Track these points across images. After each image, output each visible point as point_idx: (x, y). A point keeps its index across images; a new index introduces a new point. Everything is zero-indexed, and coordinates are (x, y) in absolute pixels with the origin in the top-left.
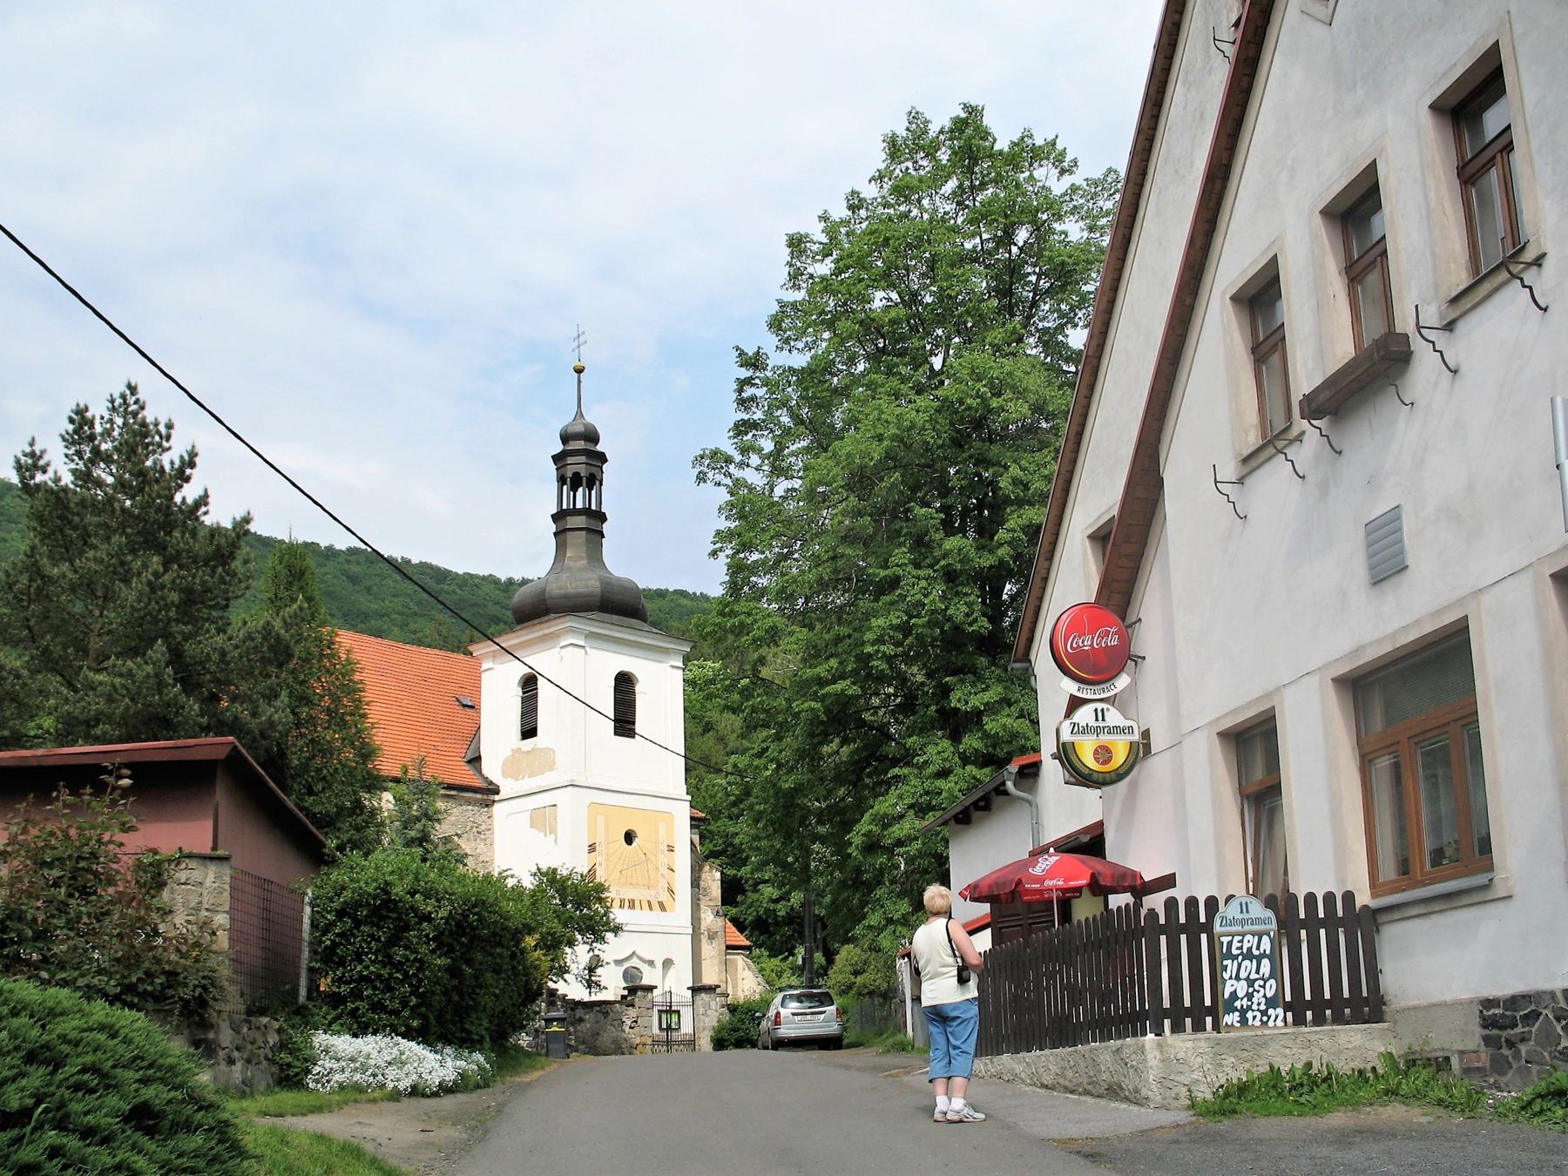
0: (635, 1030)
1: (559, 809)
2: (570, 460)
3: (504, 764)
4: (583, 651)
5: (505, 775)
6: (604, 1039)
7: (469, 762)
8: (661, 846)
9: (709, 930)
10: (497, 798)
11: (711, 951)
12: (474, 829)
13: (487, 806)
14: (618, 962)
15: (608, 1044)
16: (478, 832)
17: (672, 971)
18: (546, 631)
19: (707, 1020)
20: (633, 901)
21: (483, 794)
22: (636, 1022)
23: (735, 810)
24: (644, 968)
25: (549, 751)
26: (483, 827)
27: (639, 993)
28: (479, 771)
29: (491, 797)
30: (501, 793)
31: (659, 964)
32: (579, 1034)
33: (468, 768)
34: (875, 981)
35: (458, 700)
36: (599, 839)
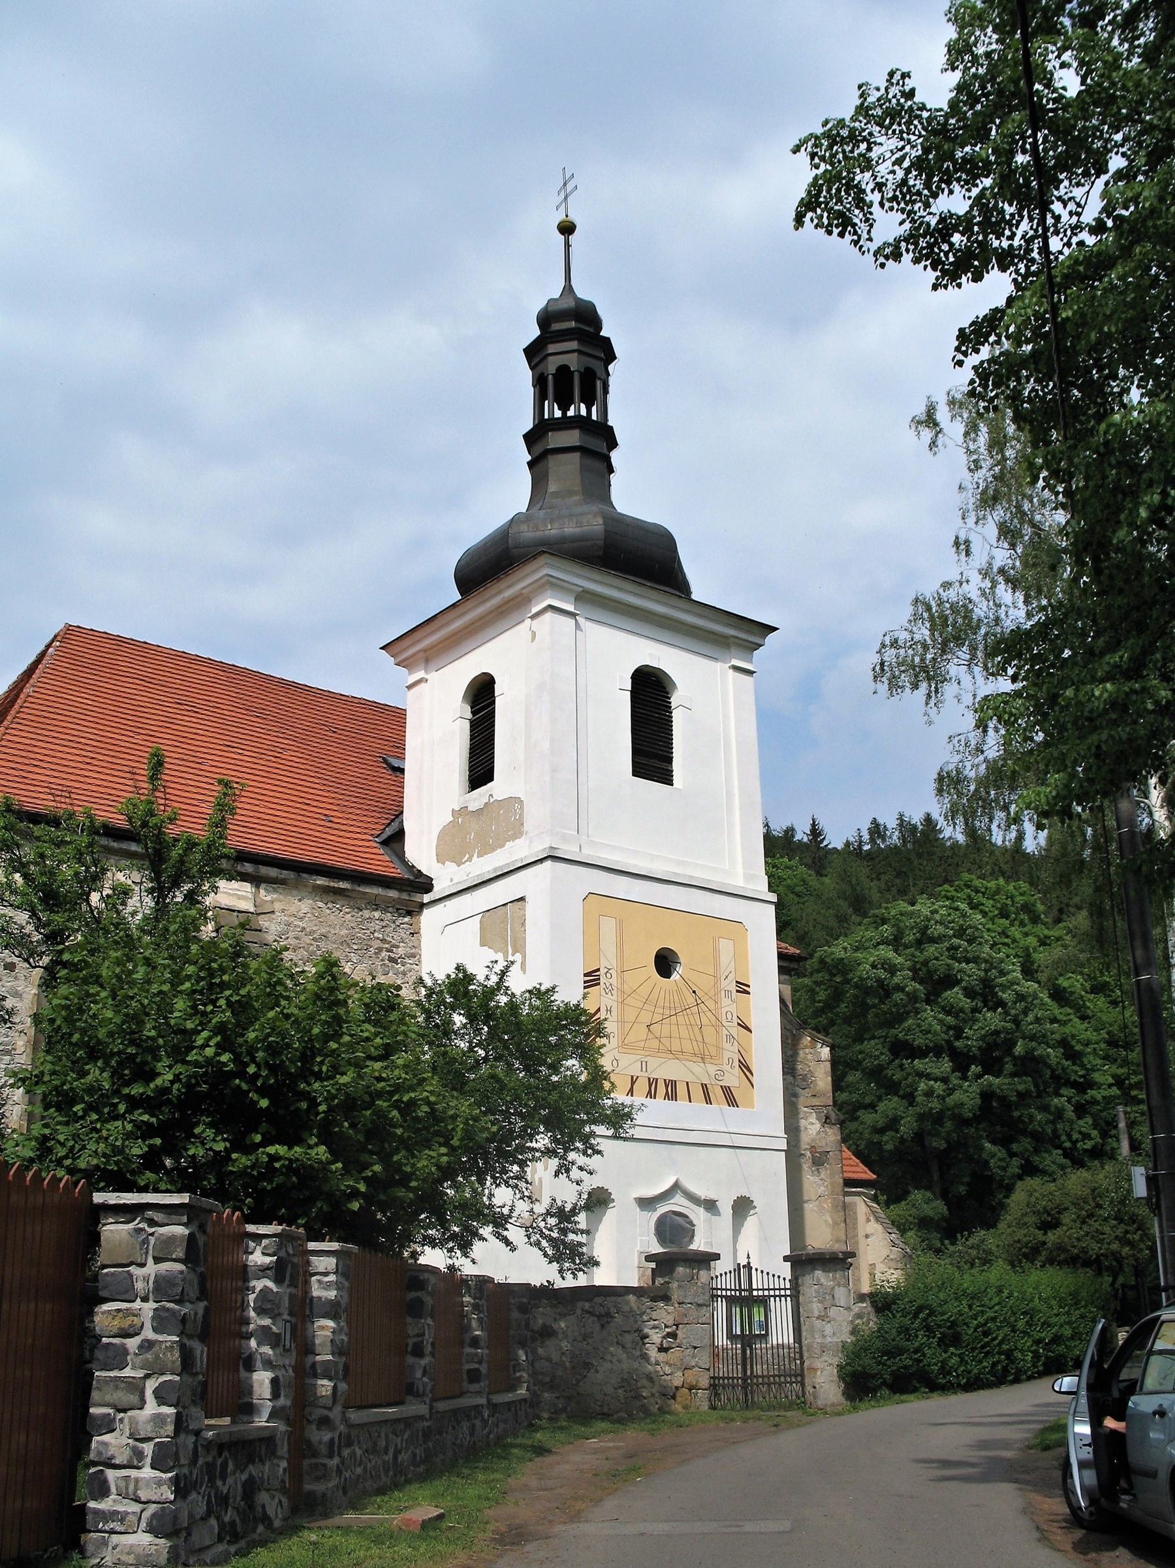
0: (674, 1355)
1: (530, 908)
2: (552, 348)
3: (441, 838)
4: (572, 622)
5: (441, 859)
6: (600, 1377)
7: (385, 843)
8: (724, 983)
9: (813, 1149)
10: (426, 898)
11: (815, 1184)
12: (384, 954)
13: (409, 913)
14: (646, 1203)
15: (610, 1390)
16: (392, 960)
17: (751, 1223)
18: (508, 593)
19: (828, 1329)
20: (674, 1083)
21: (401, 890)
22: (673, 1335)
23: (823, 1020)
24: (698, 1215)
25: (514, 802)
26: (401, 951)
27: (680, 1270)
28: (401, 855)
29: (417, 898)
30: (435, 889)
31: (726, 1208)
32: (541, 1365)
33: (382, 851)
34: (1078, 1239)
35: (385, 761)
36: (607, 960)
